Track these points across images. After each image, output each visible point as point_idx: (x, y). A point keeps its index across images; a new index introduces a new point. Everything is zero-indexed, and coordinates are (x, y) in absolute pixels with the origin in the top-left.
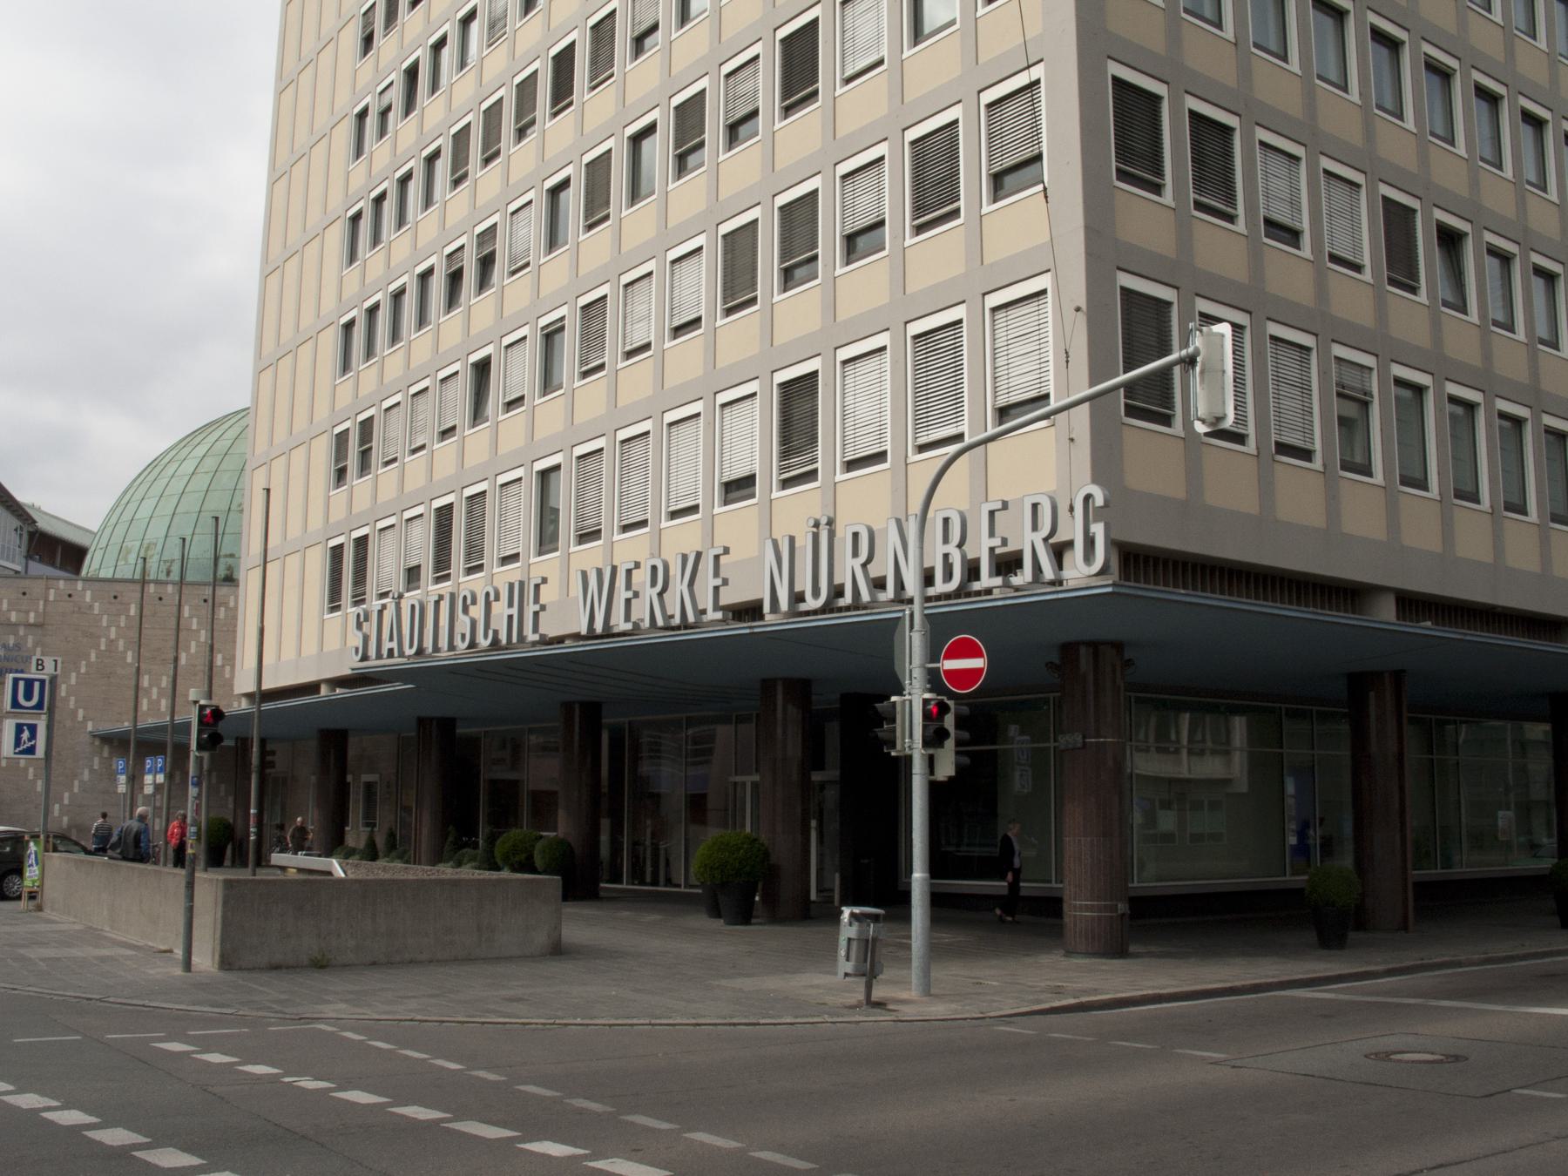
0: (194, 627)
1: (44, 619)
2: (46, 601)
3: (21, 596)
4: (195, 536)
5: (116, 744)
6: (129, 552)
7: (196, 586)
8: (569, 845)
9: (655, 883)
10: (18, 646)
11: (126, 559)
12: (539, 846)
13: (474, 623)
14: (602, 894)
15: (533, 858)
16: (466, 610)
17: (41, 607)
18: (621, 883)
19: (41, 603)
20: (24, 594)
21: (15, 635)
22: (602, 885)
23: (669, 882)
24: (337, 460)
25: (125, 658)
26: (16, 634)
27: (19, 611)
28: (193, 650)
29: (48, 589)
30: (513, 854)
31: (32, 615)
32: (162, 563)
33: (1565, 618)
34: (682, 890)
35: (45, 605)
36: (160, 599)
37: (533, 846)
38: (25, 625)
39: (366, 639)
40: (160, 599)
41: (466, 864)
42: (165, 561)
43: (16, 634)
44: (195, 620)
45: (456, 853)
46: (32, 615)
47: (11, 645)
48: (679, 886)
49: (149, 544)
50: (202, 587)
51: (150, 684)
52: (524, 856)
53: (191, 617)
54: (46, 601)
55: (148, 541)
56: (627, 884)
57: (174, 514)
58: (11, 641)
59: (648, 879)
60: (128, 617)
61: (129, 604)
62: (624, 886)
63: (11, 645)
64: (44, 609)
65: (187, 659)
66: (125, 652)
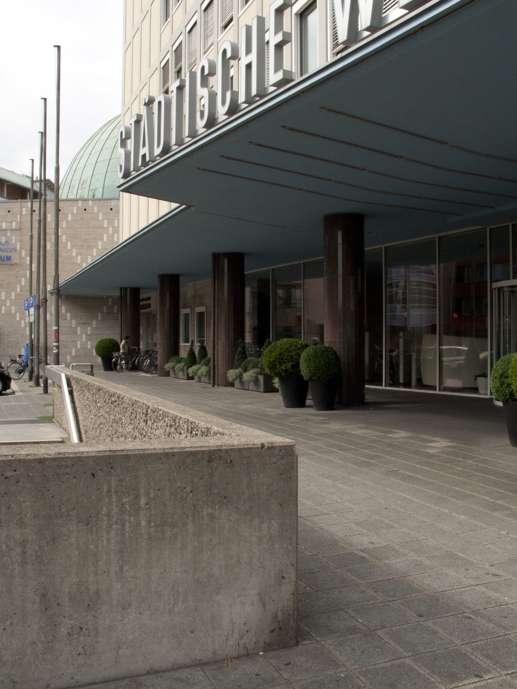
0: (106, 226)
1: (20, 226)
2: (21, 215)
3: (7, 213)
4: (107, 173)
5: (63, 297)
6: (74, 187)
7: (105, 201)
8: (335, 353)
9: (407, 384)
10: (7, 243)
11: (72, 192)
12: (304, 355)
13: (212, 97)
14: (368, 398)
15: (299, 367)
16: (205, 83)
17: (19, 219)
18: (382, 385)
19: (19, 216)
20: (9, 212)
21: (5, 236)
22: (366, 386)
23: (420, 384)
24: (164, 85)
25: (67, 246)
26: (6, 235)
27: (6, 222)
28: (105, 239)
29: (22, 208)
30: (280, 363)
31: (14, 224)
32: (90, 191)
33: (2, 425)
34: (437, 392)
35: (21, 218)
36: (85, 210)
37: (299, 355)
38: (11, 230)
39: (127, 155)
40: (85, 210)
41: (249, 370)
42: (91, 190)
43: (6, 235)
44: (106, 221)
45: (243, 361)
46: (14, 224)
47: (3, 242)
48: (433, 388)
49: (83, 182)
50: (109, 201)
51: (81, 261)
52: (289, 365)
53: (103, 220)
54: (21, 215)
55: (83, 180)
56: (386, 386)
57: (96, 162)
58: (3, 240)
59: (401, 381)
60: (67, 222)
61: (67, 214)
62: (383, 387)
63: (3, 242)
64: (20, 220)
65: (102, 245)
66: (66, 243)
